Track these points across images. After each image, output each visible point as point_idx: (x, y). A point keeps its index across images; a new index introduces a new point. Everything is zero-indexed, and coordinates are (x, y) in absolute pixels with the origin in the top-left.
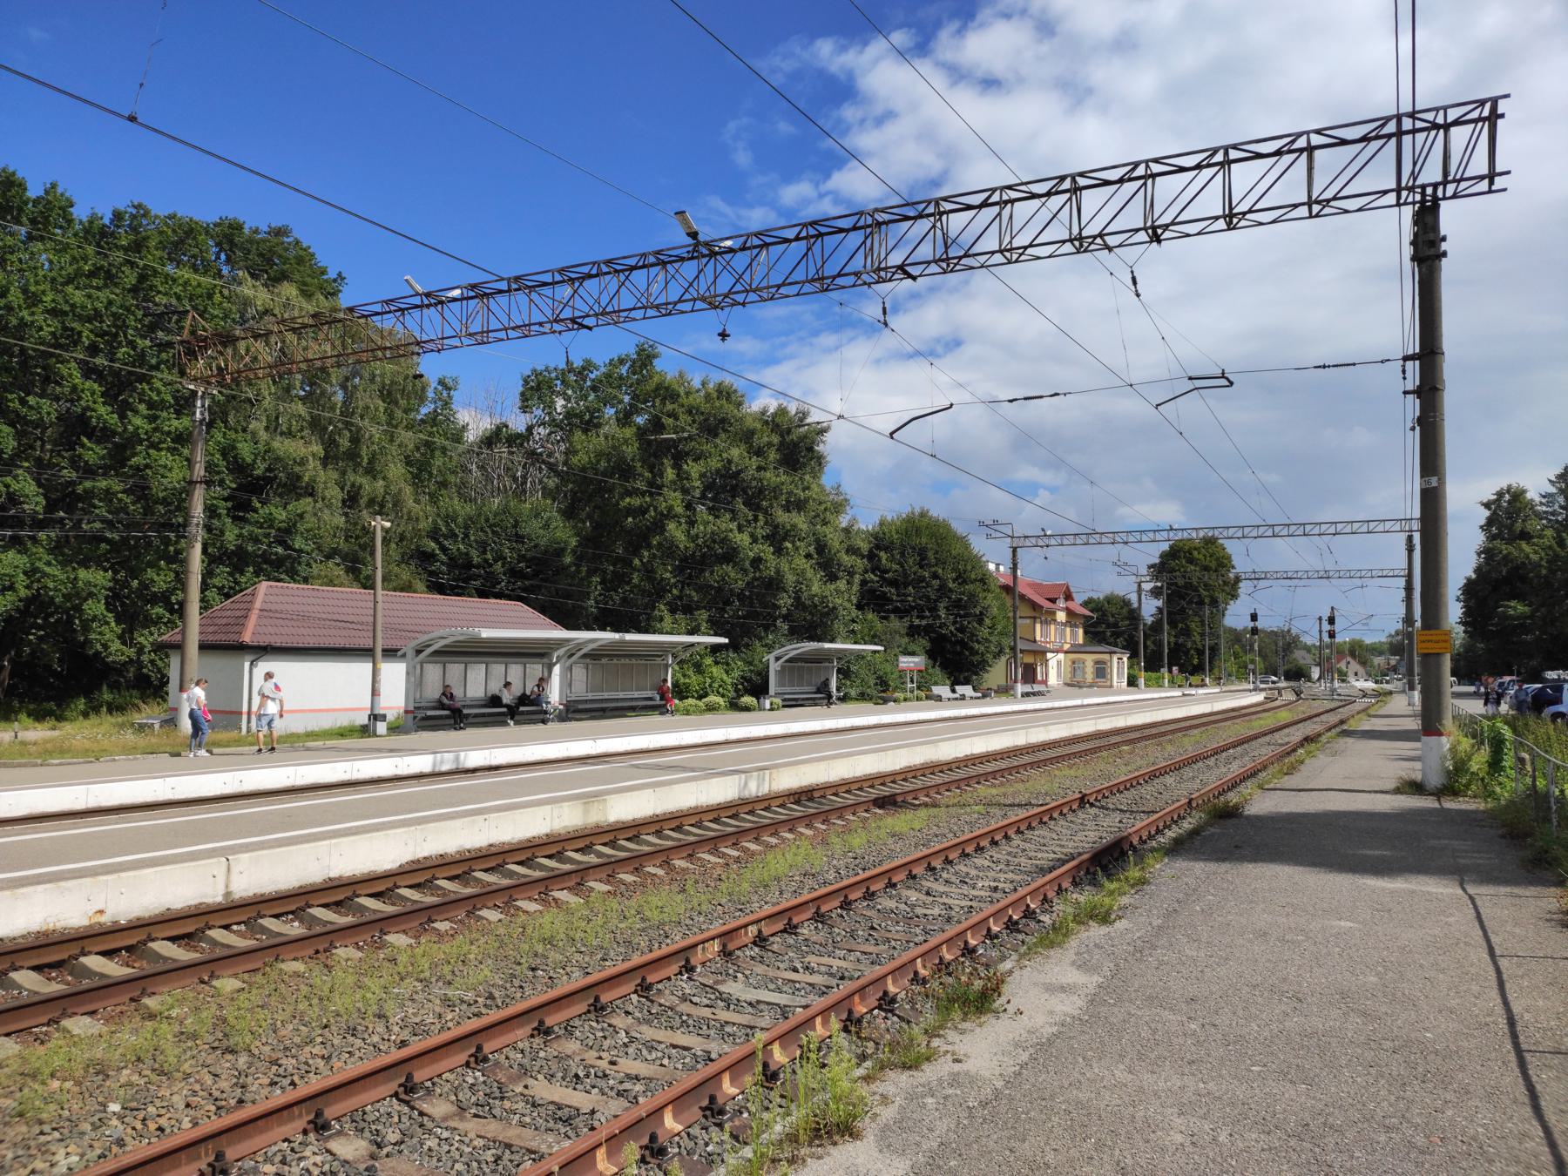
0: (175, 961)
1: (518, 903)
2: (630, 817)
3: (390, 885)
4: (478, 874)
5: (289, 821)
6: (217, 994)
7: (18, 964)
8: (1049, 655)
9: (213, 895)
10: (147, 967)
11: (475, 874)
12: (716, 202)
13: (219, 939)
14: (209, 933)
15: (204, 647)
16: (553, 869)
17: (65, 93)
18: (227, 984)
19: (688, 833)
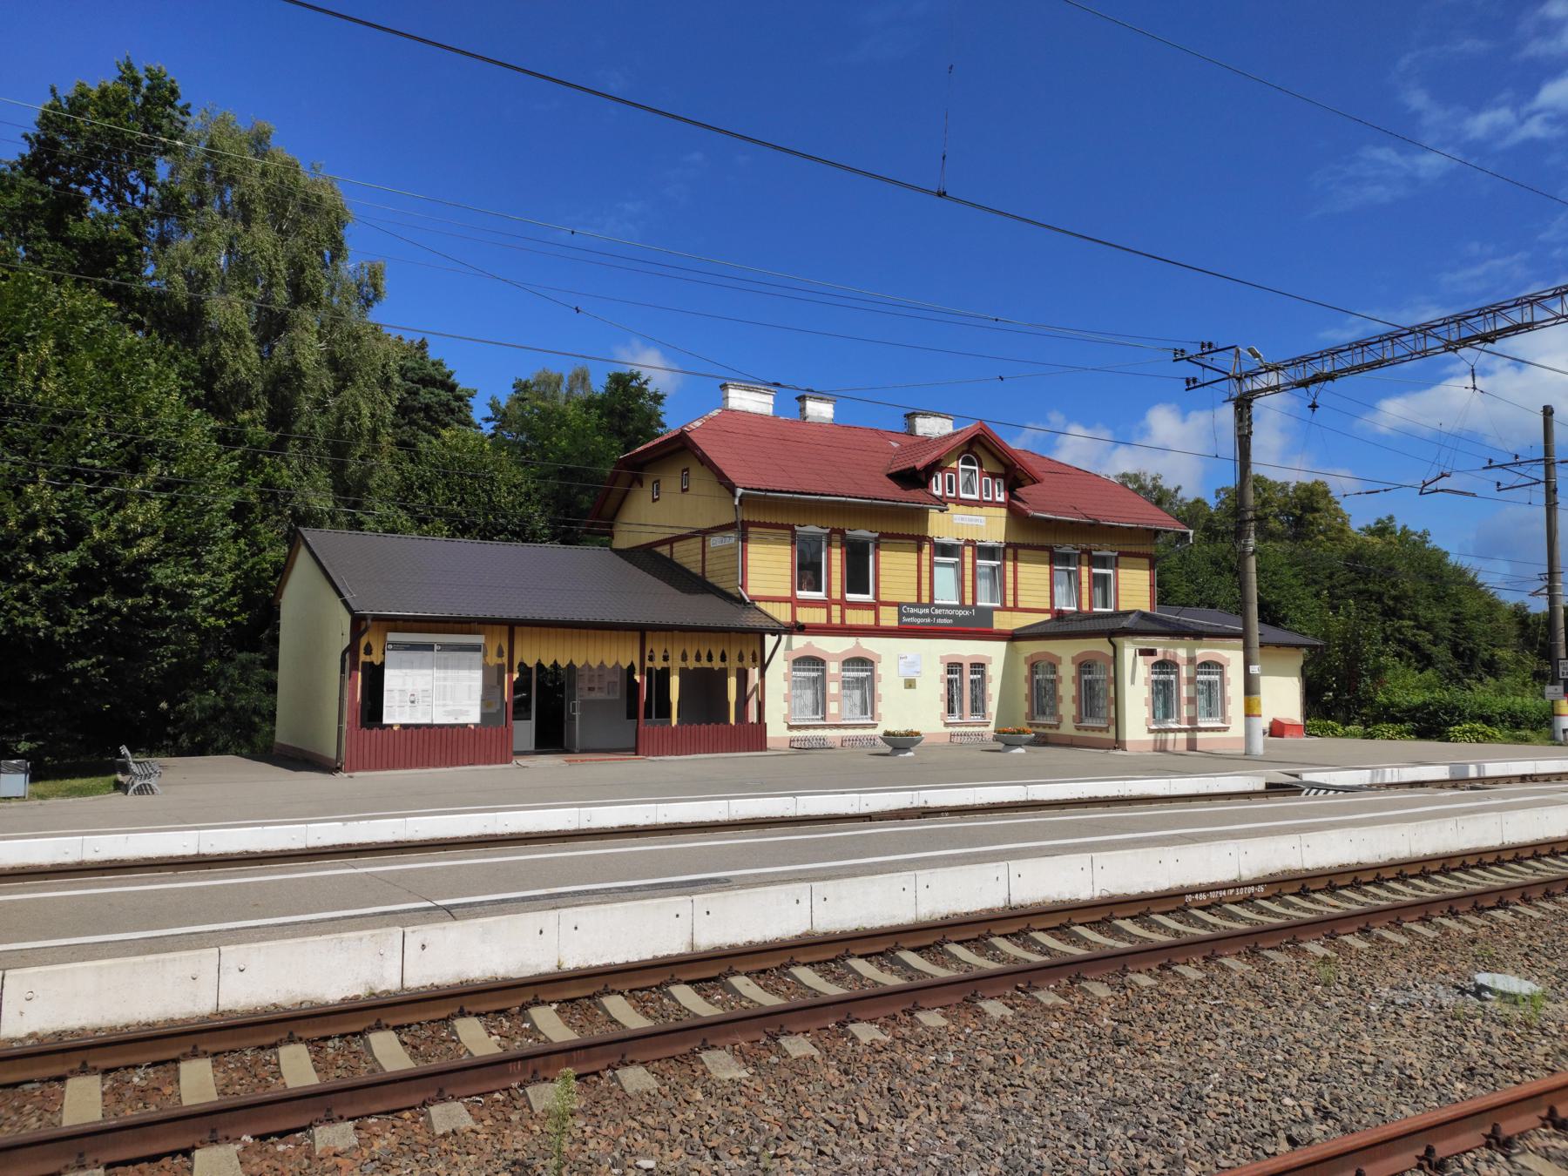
0: (696, 1016)
1: (1225, 961)
2: (1354, 860)
3: (725, 969)
4: (955, 949)
5: (183, 910)
6: (980, 1014)
7: (735, 968)
8: (770, 641)
9: (672, 944)
10: (597, 1033)
11: (1075, 928)
12: (1385, 154)
13: (744, 991)
14: (794, 970)
15: (1262, 645)
16: (1177, 932)
17: (463, 52)
18: (544, 1096)
19: (1233, 917)
